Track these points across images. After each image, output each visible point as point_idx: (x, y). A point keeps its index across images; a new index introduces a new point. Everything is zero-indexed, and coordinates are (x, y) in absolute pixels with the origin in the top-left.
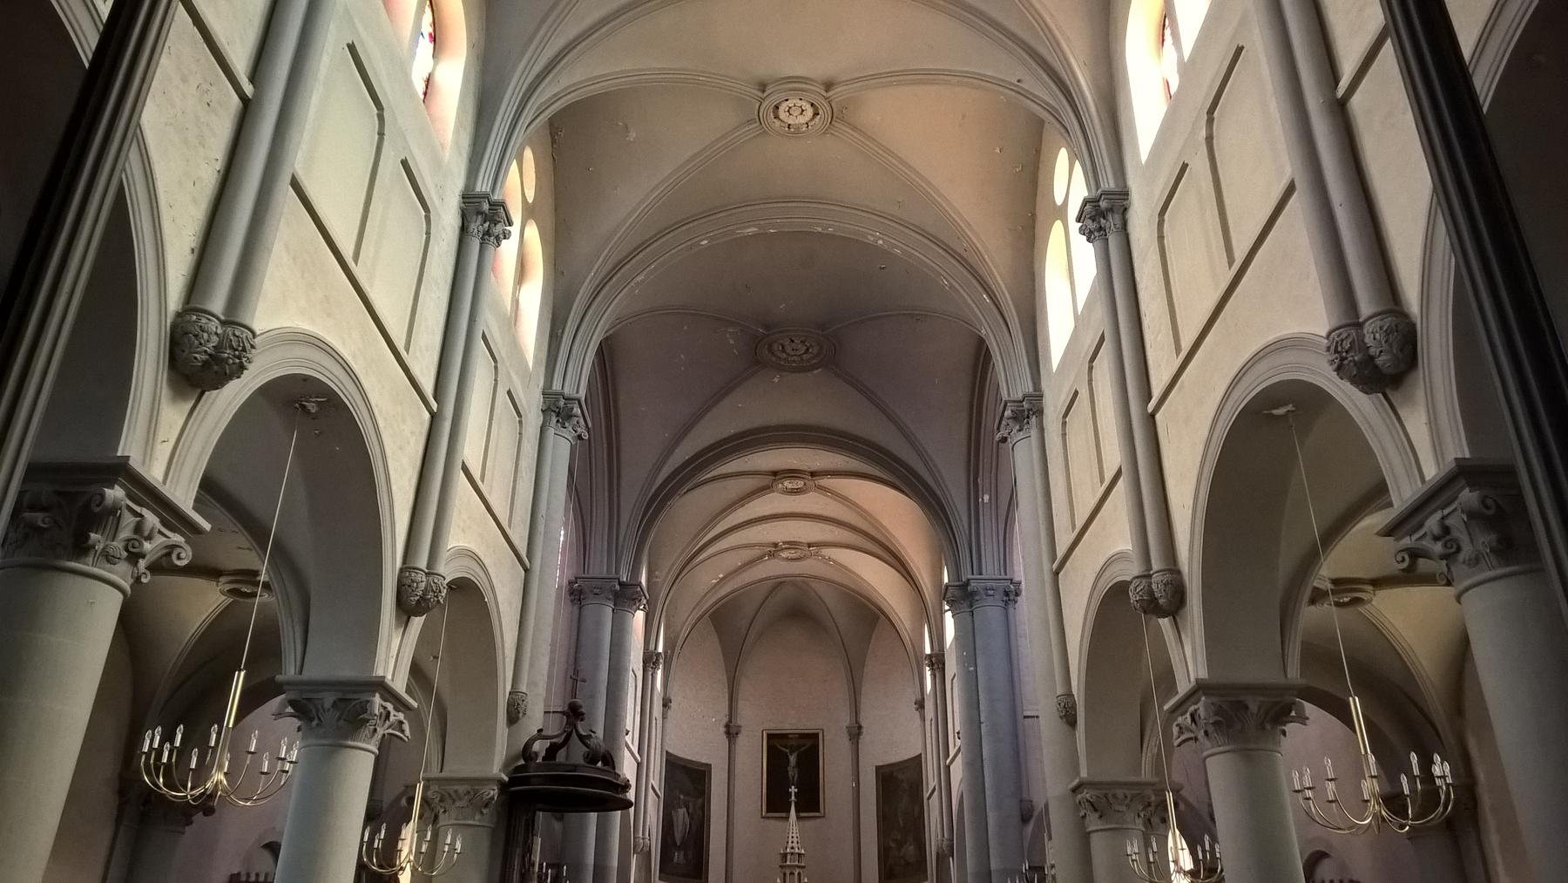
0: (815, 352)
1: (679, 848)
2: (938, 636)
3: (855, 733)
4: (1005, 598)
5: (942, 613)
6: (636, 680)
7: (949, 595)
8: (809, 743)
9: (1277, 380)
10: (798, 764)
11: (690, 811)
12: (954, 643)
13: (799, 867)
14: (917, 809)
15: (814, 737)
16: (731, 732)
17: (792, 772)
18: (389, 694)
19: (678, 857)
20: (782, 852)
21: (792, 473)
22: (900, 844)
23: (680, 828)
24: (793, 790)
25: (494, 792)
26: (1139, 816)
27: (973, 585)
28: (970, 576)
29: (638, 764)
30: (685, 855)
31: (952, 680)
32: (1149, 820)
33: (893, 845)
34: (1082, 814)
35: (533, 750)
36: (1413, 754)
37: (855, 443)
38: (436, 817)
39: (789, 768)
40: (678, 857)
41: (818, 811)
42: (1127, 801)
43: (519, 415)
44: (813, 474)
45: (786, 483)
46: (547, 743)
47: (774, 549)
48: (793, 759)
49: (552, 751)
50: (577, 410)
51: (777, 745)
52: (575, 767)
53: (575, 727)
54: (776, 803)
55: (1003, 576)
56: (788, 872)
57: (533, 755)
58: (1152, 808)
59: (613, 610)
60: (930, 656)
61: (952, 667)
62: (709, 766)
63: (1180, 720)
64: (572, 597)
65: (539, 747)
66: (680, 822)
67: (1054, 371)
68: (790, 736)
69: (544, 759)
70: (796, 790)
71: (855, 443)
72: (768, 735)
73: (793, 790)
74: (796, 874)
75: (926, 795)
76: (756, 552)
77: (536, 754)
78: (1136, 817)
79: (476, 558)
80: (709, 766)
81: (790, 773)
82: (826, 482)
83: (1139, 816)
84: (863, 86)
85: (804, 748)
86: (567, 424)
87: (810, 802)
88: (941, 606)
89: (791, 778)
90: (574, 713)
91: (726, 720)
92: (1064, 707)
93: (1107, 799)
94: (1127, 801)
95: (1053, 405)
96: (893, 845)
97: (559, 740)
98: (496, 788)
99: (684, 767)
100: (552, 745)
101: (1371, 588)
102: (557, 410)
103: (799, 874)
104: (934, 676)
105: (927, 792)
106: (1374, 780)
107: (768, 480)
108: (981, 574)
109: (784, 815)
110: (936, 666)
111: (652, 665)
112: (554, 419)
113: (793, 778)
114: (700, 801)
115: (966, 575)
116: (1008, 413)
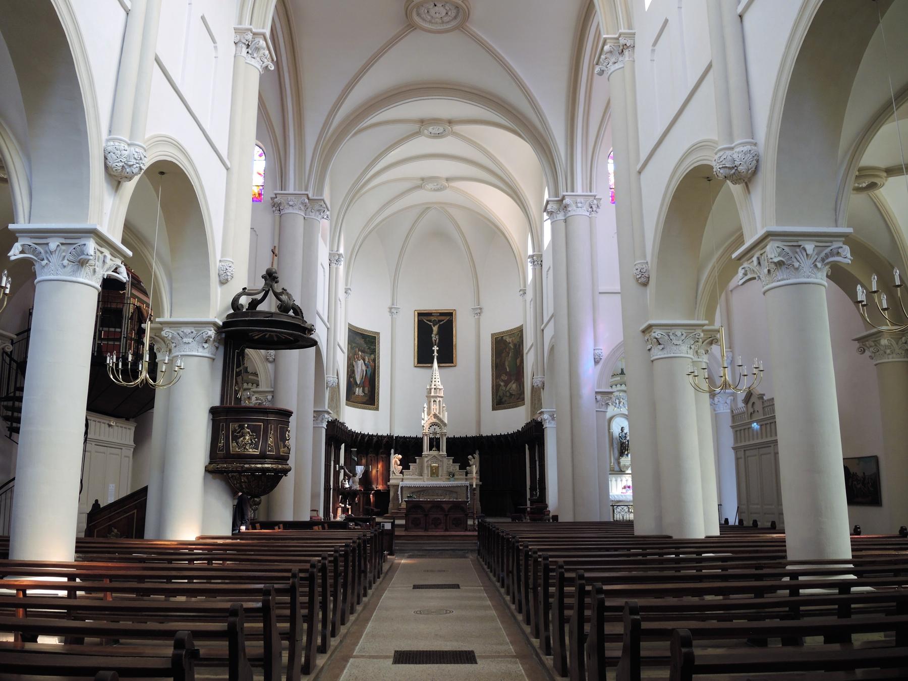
0: (454, 15)
1: (359, 386)
2: (537, 242)
3: (478, 312)
4: (590, 209)
5: (542, 221)
6: (324, 271)
7: (549, 207)
8: (447, 318)
9: (697, 165)
10: (439, 333)
11: (366, 362)
12: (551, 242)
13: (439, 397)
14: (518, 361)
15: (450, 314)
16: (392, 310)
17: (435, 337)
18: (102, 240)
19: (358, 391)
20: (428, 387)
21: (435, 121)
22: (507, 383)
23: (359, 373)
24: (435, 348)
25: (212, 332)
26: (691, 348)
27: (567, 201)
28: (565, 193)
29: (328, 329)
30: (363, 391)
31: (548, 271)
32: (697, 352)
33: (502, 384)
34: (649, 347)
35: (240, 303)
36: (526, 445)
37: (426, 409)
38: (170, 351)
39: (433, 335)
40: (358, 391)
41: (453, 363)
42: (683, 338)
43: (214, 42)
44: (450, 122)
45: (430, 129)
46: (250, 299)
47: (423, 182)
48: (435, 329)
49: (254, 304)
50: (262, 43)
51: (425, 321)
52: (271, 314)
53: (271, 287)
54: (424, 358)
55: (589, 194)
56: (432, 400)
57: (239, 306)
58: (700, 344)
59: (304, 218)
60: (532, 256)
61: (547, 262)
62: (378, 334)
63: (745, 265)
64: (274, 208)
65: (244, 301)
66: (359, 369)
67: (529, 283)
68: (433, 314)
69: (247, 309)
70: (438, 348)
71: (426, 409)
72: (418, 313)
73: (435, 348)
74: (438, 401)
75: (525, 351)
76: (407, 185)
77: (242, 305)
78: (689, 349)
79: (175, 143)
80: (378, 334)
81: (434, 339)
82: (457, 128)
83: (691, 348)
84: (466, 12)
85: (443, 322)
86: (255, 55)
87: (447, 357)
88: (542, 217)
89: (434, 342)
90: (271, 277)
91: (389, 304)
92: (640, 271)
93: (669, 336)
94: (683, 338)
95: (643, 43)
96: (502, 384)
97: (259, 297)
98: (212, 329)
99: (362, 334)
100: (253, 300)
101: (885, 174)
102: (247, 43)
103: (439, 401)
104: (534, 270)
105: (526, 348)
106: (707, 380)
107: (416, 127)
108: (573, 191)
109: (430, 365)
110: (536, 263)
111: (335, 262)
112: (244, 50)
113: (435, 341)
114: (373, 356)
115: (562, 193)
116: (607, 48)
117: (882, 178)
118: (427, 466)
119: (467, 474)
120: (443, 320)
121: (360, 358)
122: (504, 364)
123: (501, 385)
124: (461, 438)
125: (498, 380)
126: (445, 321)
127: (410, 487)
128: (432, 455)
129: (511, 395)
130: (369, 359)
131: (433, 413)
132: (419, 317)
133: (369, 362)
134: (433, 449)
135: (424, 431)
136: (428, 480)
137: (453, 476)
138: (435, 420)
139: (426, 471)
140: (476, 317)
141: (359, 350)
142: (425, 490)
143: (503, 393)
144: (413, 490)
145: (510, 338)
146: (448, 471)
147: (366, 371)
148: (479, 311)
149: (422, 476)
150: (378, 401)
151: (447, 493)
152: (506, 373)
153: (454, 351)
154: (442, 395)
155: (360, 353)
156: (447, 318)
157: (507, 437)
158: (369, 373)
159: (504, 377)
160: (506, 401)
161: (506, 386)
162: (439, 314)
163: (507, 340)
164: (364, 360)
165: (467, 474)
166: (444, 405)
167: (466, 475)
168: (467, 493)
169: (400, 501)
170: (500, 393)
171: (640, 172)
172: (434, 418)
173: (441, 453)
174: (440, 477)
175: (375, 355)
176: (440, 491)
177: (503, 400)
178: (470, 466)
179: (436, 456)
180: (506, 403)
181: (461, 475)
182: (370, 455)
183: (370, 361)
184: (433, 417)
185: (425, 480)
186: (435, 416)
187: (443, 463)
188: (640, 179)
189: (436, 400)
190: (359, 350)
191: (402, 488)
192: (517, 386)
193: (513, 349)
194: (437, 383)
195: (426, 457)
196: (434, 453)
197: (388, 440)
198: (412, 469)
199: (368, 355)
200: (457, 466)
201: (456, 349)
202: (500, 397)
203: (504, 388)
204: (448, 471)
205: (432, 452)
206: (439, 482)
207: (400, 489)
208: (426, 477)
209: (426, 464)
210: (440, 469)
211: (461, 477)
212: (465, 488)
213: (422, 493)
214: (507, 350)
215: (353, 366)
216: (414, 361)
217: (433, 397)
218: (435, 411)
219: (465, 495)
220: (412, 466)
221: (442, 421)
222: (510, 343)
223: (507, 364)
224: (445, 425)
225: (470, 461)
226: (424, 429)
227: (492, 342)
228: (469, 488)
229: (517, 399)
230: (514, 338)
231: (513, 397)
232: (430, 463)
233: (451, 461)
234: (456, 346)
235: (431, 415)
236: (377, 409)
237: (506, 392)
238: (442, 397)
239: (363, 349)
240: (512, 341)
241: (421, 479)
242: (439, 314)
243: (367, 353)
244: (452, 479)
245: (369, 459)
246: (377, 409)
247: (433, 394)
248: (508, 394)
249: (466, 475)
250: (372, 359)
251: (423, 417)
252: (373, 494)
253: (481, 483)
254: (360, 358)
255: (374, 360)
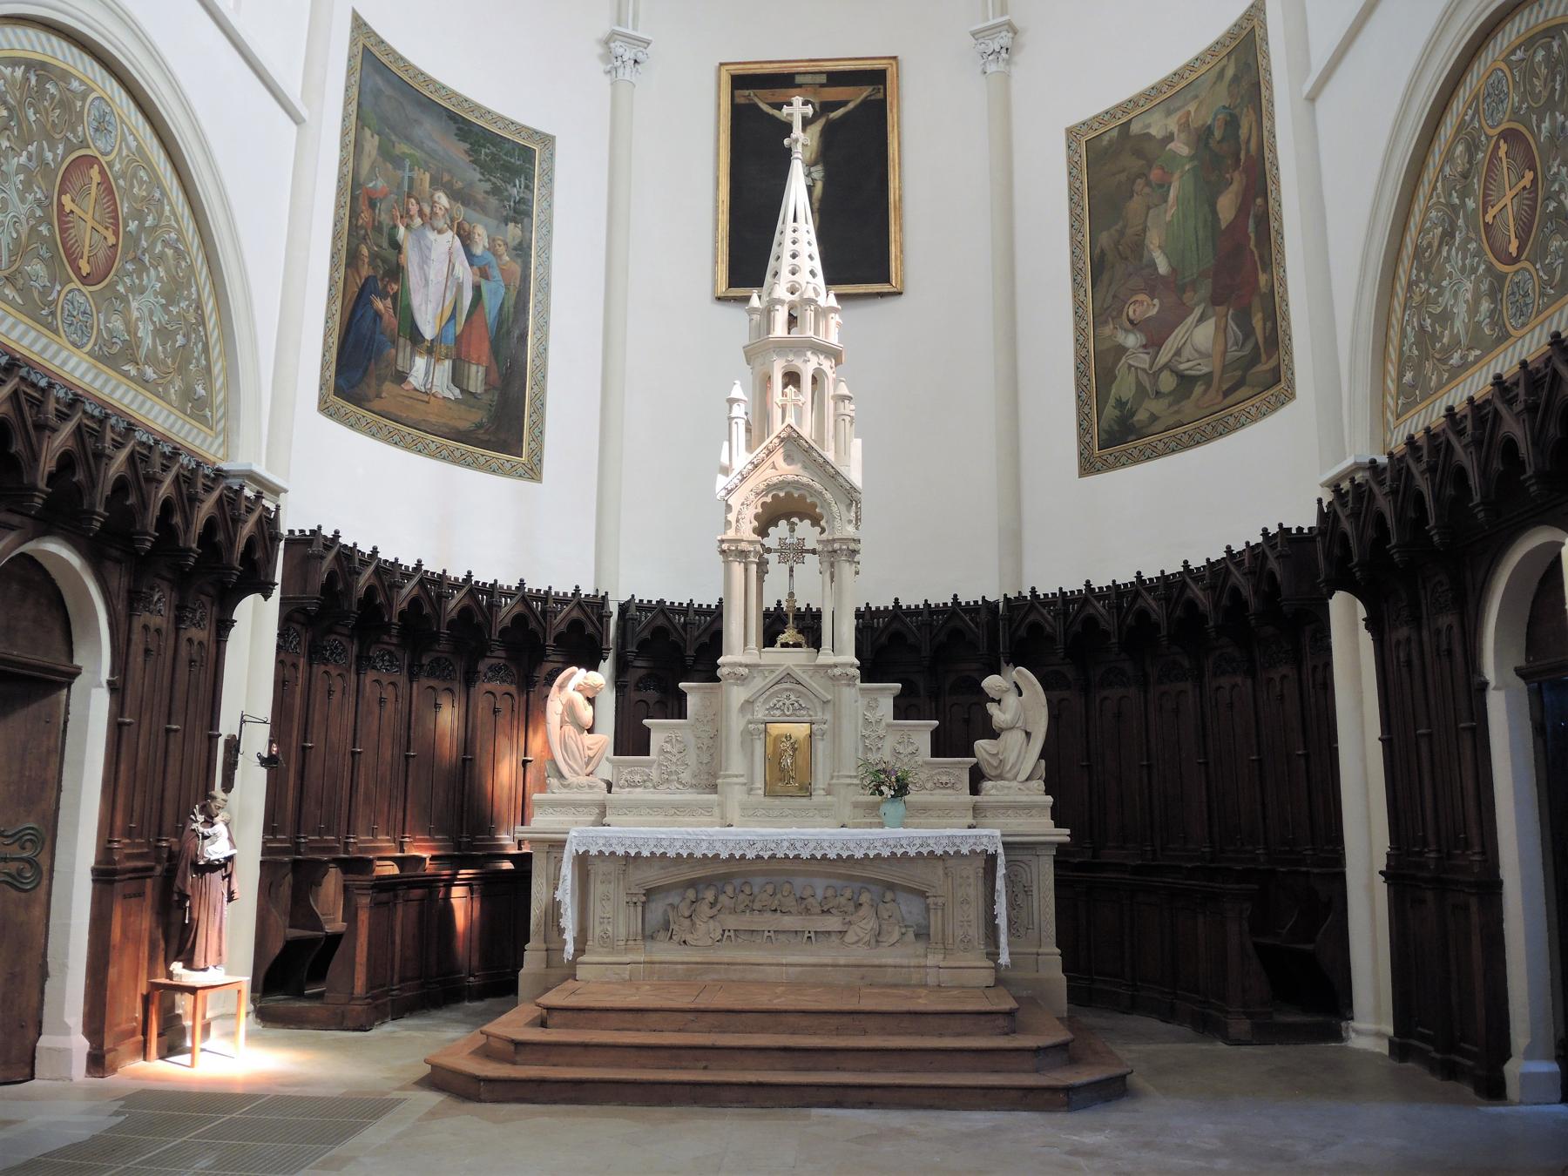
8: (862, 93)
11: (478, 250)
15: (875, 78)
30: (457, 378)
33: (1132, 340)
41: (887, 280)
62: (548, 140)
66: (437, 271)
68: (799, 79)
96: (1132, 340)
99: (452, 117)
114: (513, 231)
117: (399, 1101)
118: (748, 736)
119: (977, 778)
120: (844, 103)
121: (441, 224)
122: (1139, 246)
123: (1121, 350)
124: (929, 610)
125: (1107, 330)
126: (851, 106)
127: (631, 861)
128: (772, 668)
129: (1186, 382)
130: (492, 240)
131: (778, 427)
132: (738, 92)
133: (492, 249)
134: (782, 638)
135: (731, 534)
136: (749, 812)
137: (901, 789)
138: (782, 469)
139: (736, 763)
140: (991, 68)
141: (436, 183)
142: (727, 878)
143: (1139, 384)
144: (653, 876)
145: (1169, 113)
146: (866, 763)
147: (477, 289)
148: (1004, 39)
149: (714, 788)
150: (539, 437)
151: (865, 898)
152: (1153, 284)
153: (892, 228)
154: (833, 339)
155: (443, 200)
156: (862, 93)
157: (1227, 571)
158: (491, 304)
159: (1145, 307)
160: (1154, 418)
161: (1154, 344)
162: (823, 79)
163: (1153, 131)
164: (466, 239)
165: (977, 778)
166: (844, 390)
167: (975, 790)
168: (990, 902)
169: (570, 948)
170: (1124, 387)
171: (1312, 99)
172: (788, 458)
173: (826, 657)
174: (819, 796)
175: (527, 230)
176: (820, 886)
177: (1141, 416)
178: (994, 734)
179: (799, 673)
180: (1158, 426)
181: (944, 786)
182: (488, 686)
183: (502, 249)
184: (778, 457)
185: (734, 814)
186: (793, 444)
187: (837, 717)
188: (1314, 109)
189: (798, 363)
190: (436, 183)
191: (582, 860)
192: (1222, 330)
193: (1192, 158)
194: (803, 277)
195: (742, 680)
196: (789, 657)
197: (576, 614)
198: (663, 751)
199: (493, 222)
200: (921, 732)
201: (900, 217)
202: (1120, 404)
203: (1143, 360)
204: (866, 763)
205: (774, 655)
206: (810, 832)
207: (567, 870)
208: (735, 796)
209: (736, 724)
210: (821, 747)
211: (939, 797)
212: (978, 866)
213: (709, 895)
214: (1155, 175)
215: (396, 246)
216: (715, 273)
217: (783, 347)
218: (790, 420)
219: (975, 912)
220: (660, 730)
221: (832, 476)
222: (1170, 138)
223: (1154, 240)
224: (850, 496)
225: (992, 708)
226: (728, 524)
227: (1072, 165)
228: (1001, 871)
229: (1226, 394)
230: (1192, 108)
231: (1198, 389)
232: (760, 714)
233: (887, 705)
234: (899, 209)
235: (771, 440)
236: (533, 472)
237: (1156, 375)
238: (834, 354)
239: (459, 185)
240: (1185, 125)
241: (707, 809)
242: (823, 79)
243: (483, 209)
244: (893, 810)
245: (482, 704)
246: (533, 472)
247: (780, 329)
248: (1167, 382)
249: (975, 790)
250: (512, 244)
251: (725, 459)
252: (469, 883)
253: (1063, 835)
254: (441, 224)
255: (522, 250)
